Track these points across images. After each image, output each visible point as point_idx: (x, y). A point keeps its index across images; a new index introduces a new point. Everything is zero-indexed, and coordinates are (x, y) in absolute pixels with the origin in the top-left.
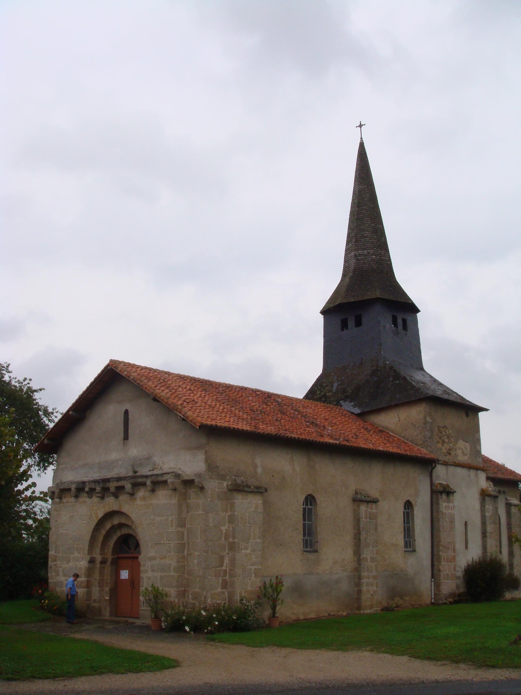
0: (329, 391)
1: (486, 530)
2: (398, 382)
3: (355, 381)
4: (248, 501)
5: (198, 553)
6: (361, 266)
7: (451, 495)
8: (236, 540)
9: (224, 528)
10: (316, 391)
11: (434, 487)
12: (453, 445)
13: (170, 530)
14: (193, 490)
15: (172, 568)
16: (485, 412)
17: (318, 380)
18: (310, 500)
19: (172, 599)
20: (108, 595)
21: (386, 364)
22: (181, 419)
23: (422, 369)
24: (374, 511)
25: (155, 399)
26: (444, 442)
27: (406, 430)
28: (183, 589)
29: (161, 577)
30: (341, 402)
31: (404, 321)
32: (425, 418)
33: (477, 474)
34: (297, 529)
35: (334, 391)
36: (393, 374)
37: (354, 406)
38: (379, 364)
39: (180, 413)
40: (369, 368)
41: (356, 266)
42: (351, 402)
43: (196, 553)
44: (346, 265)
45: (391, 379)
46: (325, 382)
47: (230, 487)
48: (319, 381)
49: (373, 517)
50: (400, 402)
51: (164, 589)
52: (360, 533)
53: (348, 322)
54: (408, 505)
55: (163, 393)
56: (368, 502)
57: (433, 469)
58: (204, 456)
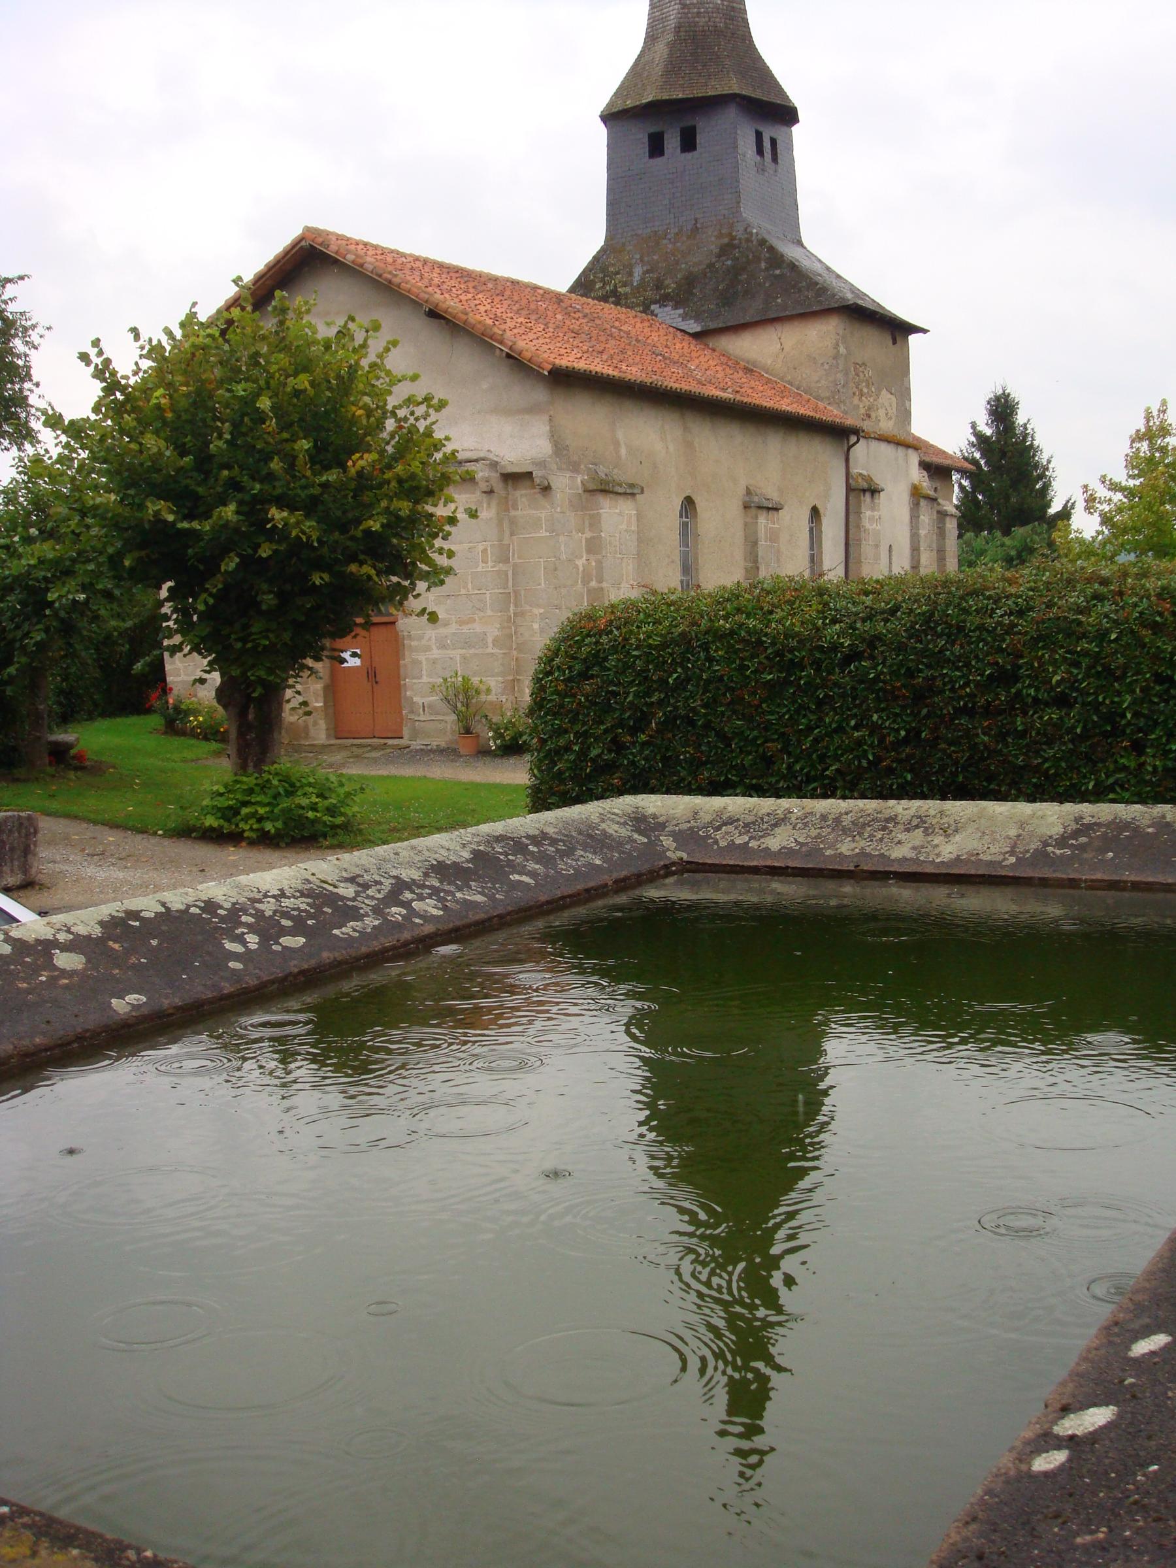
0: (625, 285)
1: (919, 561)
2: (777, 272)
3: (683, 266)
4: (617, 511)
5: (542, 611)
6: (691, 20)
7: (877, 494)
8: (604, 585)
9: (580, 563)
10: (593, 282)
11: (851, 481)
12: (875, 400)
13: (479, 569)
14: (523, 492)
15: (490, 640)
16: (920, 335)
17: (596, 259)
18: (689, 504)
19: (492, 697)
20: (321, 699)
21: (751, 233)
22: (504, 355)
23: (800, 243)
24: (776, 526)
25: (434, 314)
26: (861, 394)
27: (795, 369)
28: (511, 678)
29: (464, 658)
30: (653, 307)
31: (773, 142)
32: (836, 346)
33: (906, 455)
34: (673, 562)
35: (635, 284)
36: (767, 255)
37: (684, 317)
38: (734, 234)
39: (501, 343)
40: (713, 239)
41: (682, 20)
42: (676, 308)
43: (536, 611)
44: (657, 14)
45: (763, 265)
46: (613, 265)
47: (592, 486)
48: (598, 261)
49: (774, 537)
50: (788, 313)
51: (484, 679)
52: (758, 568)
53: (665, 142)
54: (815, 513)
55: (451, 301)
56: (769, 509)
57: (850, 447)
58: (548, 428)
